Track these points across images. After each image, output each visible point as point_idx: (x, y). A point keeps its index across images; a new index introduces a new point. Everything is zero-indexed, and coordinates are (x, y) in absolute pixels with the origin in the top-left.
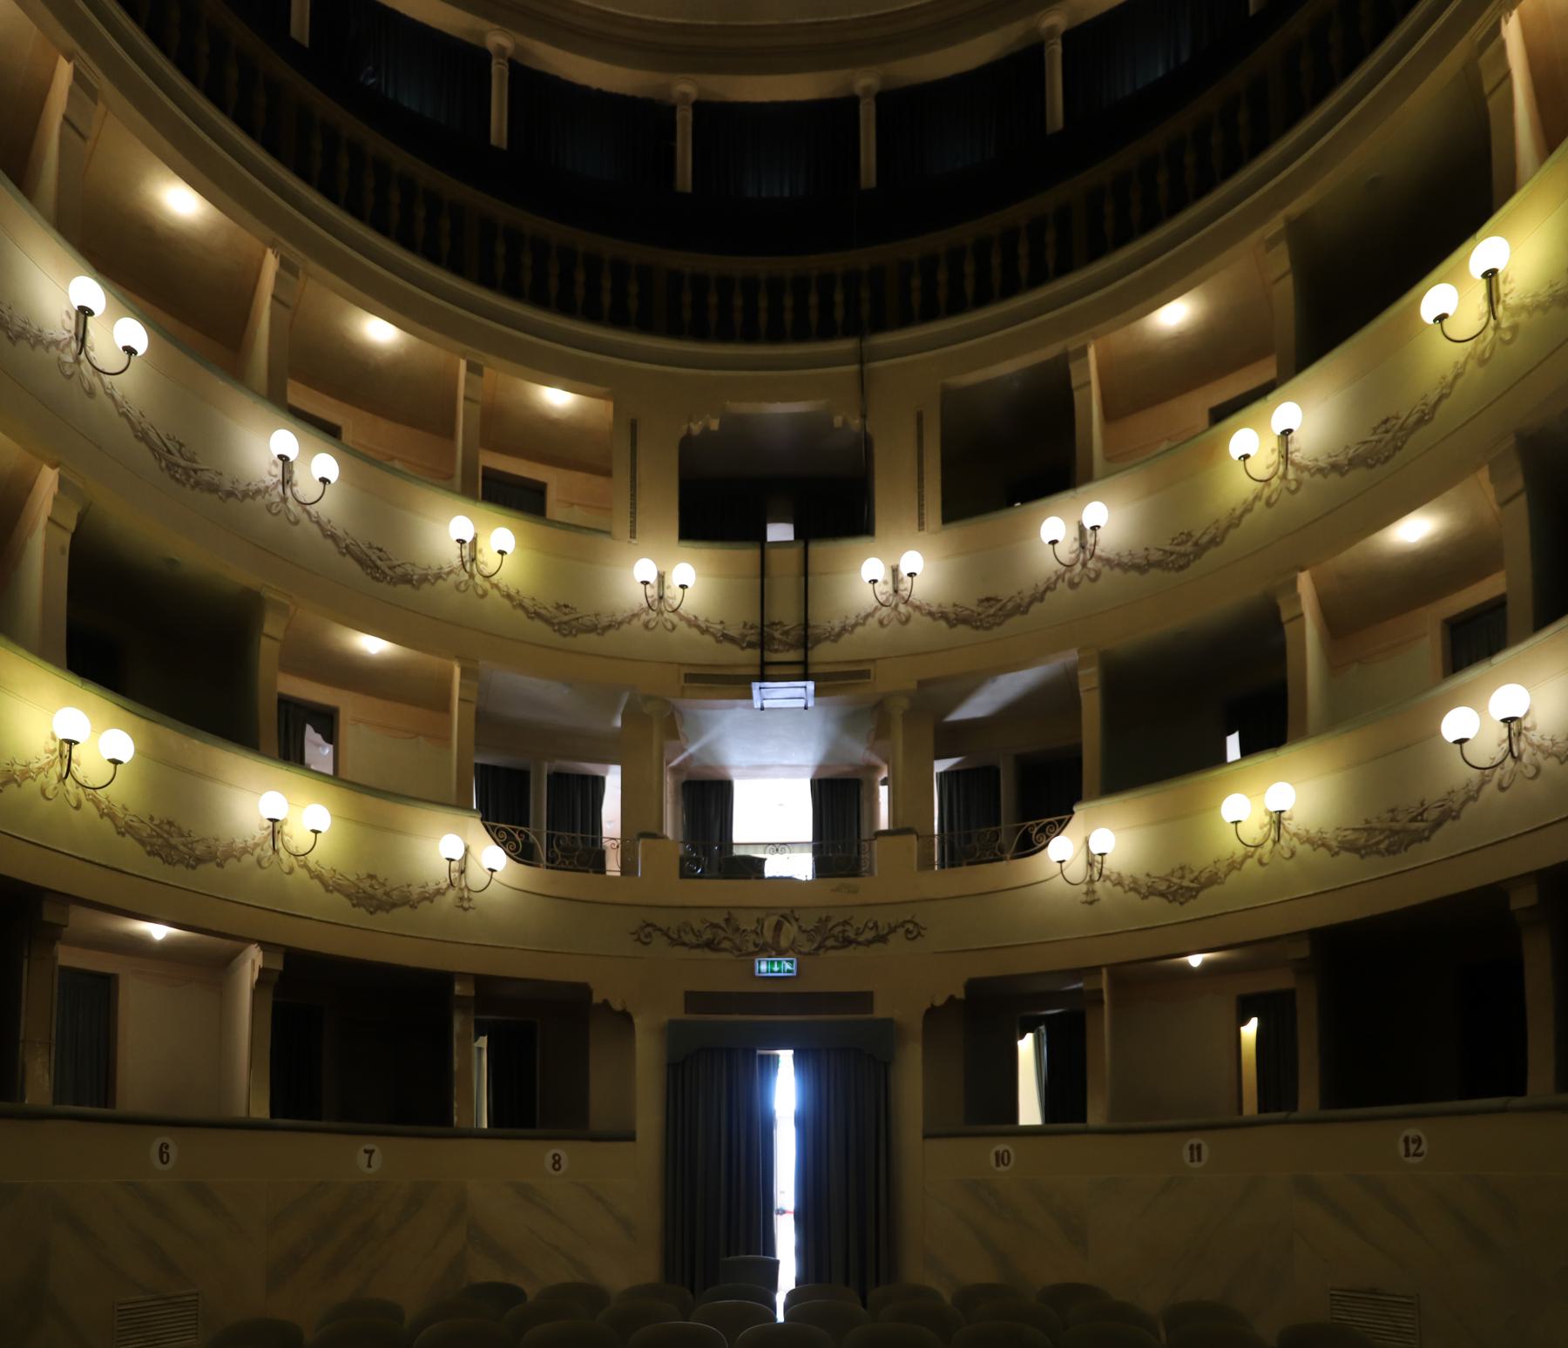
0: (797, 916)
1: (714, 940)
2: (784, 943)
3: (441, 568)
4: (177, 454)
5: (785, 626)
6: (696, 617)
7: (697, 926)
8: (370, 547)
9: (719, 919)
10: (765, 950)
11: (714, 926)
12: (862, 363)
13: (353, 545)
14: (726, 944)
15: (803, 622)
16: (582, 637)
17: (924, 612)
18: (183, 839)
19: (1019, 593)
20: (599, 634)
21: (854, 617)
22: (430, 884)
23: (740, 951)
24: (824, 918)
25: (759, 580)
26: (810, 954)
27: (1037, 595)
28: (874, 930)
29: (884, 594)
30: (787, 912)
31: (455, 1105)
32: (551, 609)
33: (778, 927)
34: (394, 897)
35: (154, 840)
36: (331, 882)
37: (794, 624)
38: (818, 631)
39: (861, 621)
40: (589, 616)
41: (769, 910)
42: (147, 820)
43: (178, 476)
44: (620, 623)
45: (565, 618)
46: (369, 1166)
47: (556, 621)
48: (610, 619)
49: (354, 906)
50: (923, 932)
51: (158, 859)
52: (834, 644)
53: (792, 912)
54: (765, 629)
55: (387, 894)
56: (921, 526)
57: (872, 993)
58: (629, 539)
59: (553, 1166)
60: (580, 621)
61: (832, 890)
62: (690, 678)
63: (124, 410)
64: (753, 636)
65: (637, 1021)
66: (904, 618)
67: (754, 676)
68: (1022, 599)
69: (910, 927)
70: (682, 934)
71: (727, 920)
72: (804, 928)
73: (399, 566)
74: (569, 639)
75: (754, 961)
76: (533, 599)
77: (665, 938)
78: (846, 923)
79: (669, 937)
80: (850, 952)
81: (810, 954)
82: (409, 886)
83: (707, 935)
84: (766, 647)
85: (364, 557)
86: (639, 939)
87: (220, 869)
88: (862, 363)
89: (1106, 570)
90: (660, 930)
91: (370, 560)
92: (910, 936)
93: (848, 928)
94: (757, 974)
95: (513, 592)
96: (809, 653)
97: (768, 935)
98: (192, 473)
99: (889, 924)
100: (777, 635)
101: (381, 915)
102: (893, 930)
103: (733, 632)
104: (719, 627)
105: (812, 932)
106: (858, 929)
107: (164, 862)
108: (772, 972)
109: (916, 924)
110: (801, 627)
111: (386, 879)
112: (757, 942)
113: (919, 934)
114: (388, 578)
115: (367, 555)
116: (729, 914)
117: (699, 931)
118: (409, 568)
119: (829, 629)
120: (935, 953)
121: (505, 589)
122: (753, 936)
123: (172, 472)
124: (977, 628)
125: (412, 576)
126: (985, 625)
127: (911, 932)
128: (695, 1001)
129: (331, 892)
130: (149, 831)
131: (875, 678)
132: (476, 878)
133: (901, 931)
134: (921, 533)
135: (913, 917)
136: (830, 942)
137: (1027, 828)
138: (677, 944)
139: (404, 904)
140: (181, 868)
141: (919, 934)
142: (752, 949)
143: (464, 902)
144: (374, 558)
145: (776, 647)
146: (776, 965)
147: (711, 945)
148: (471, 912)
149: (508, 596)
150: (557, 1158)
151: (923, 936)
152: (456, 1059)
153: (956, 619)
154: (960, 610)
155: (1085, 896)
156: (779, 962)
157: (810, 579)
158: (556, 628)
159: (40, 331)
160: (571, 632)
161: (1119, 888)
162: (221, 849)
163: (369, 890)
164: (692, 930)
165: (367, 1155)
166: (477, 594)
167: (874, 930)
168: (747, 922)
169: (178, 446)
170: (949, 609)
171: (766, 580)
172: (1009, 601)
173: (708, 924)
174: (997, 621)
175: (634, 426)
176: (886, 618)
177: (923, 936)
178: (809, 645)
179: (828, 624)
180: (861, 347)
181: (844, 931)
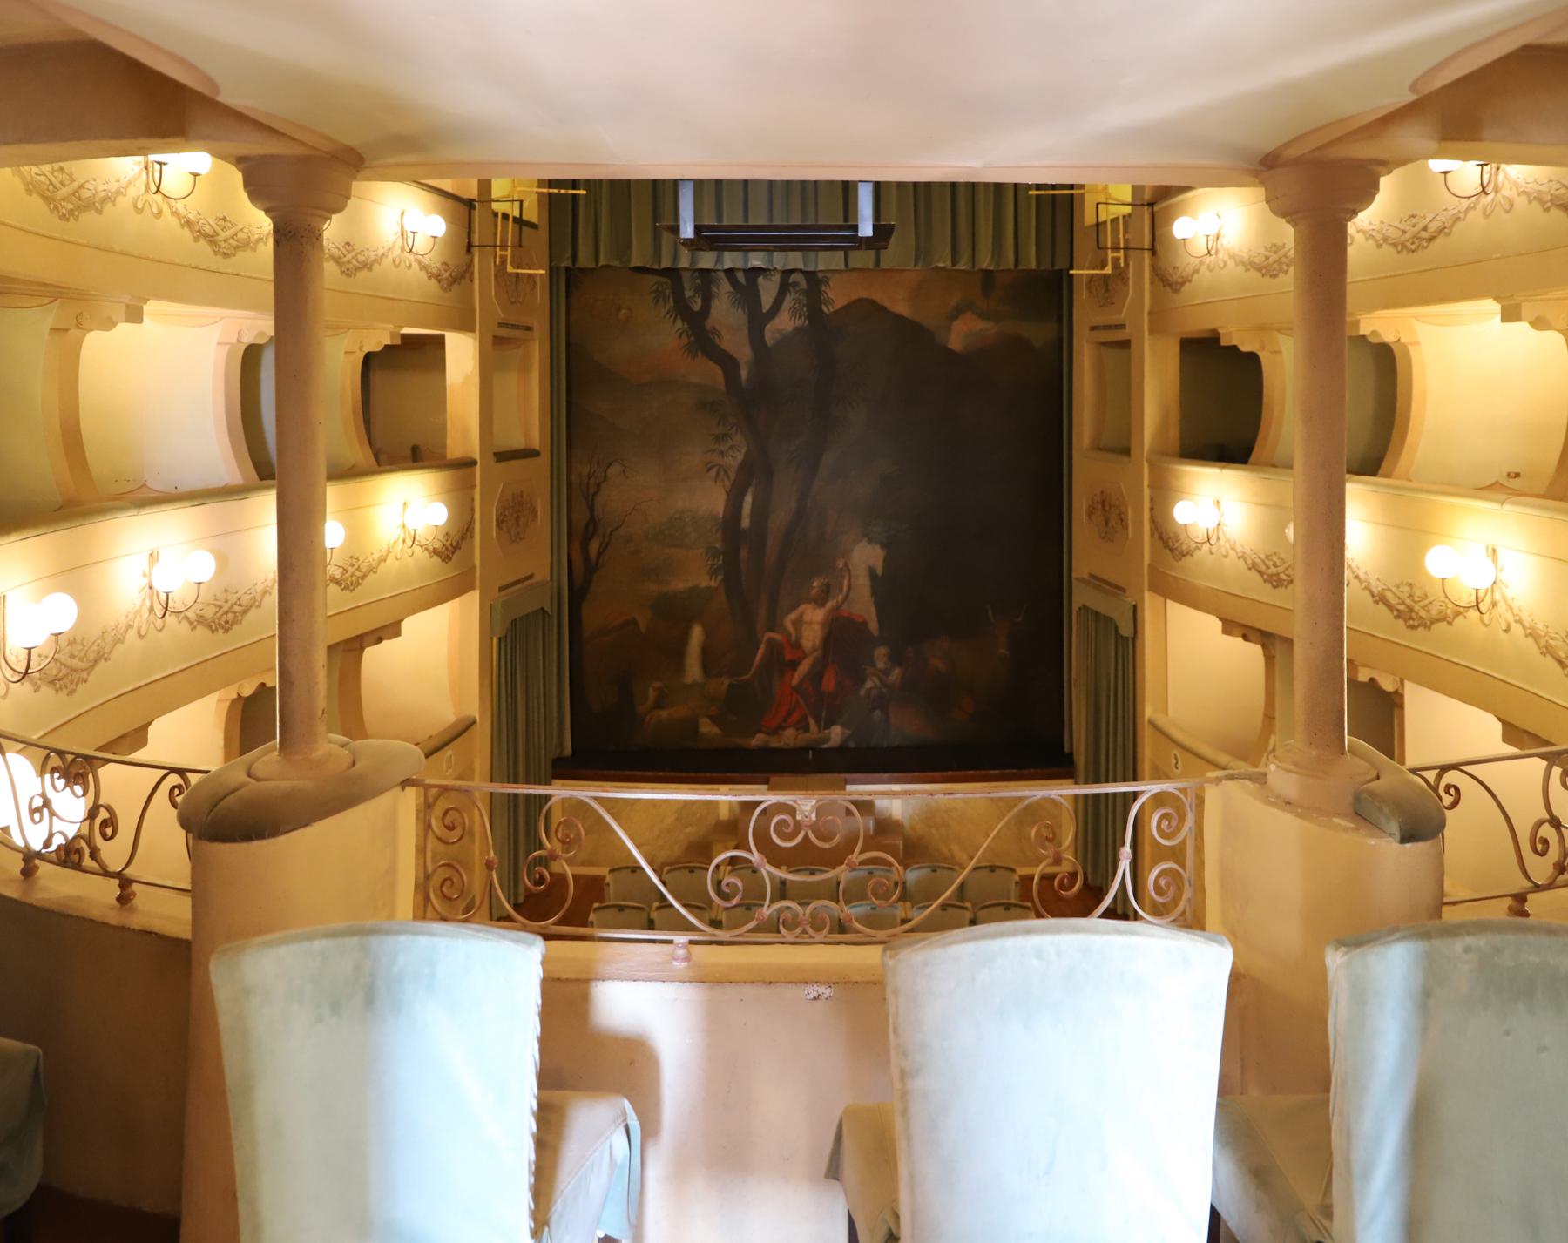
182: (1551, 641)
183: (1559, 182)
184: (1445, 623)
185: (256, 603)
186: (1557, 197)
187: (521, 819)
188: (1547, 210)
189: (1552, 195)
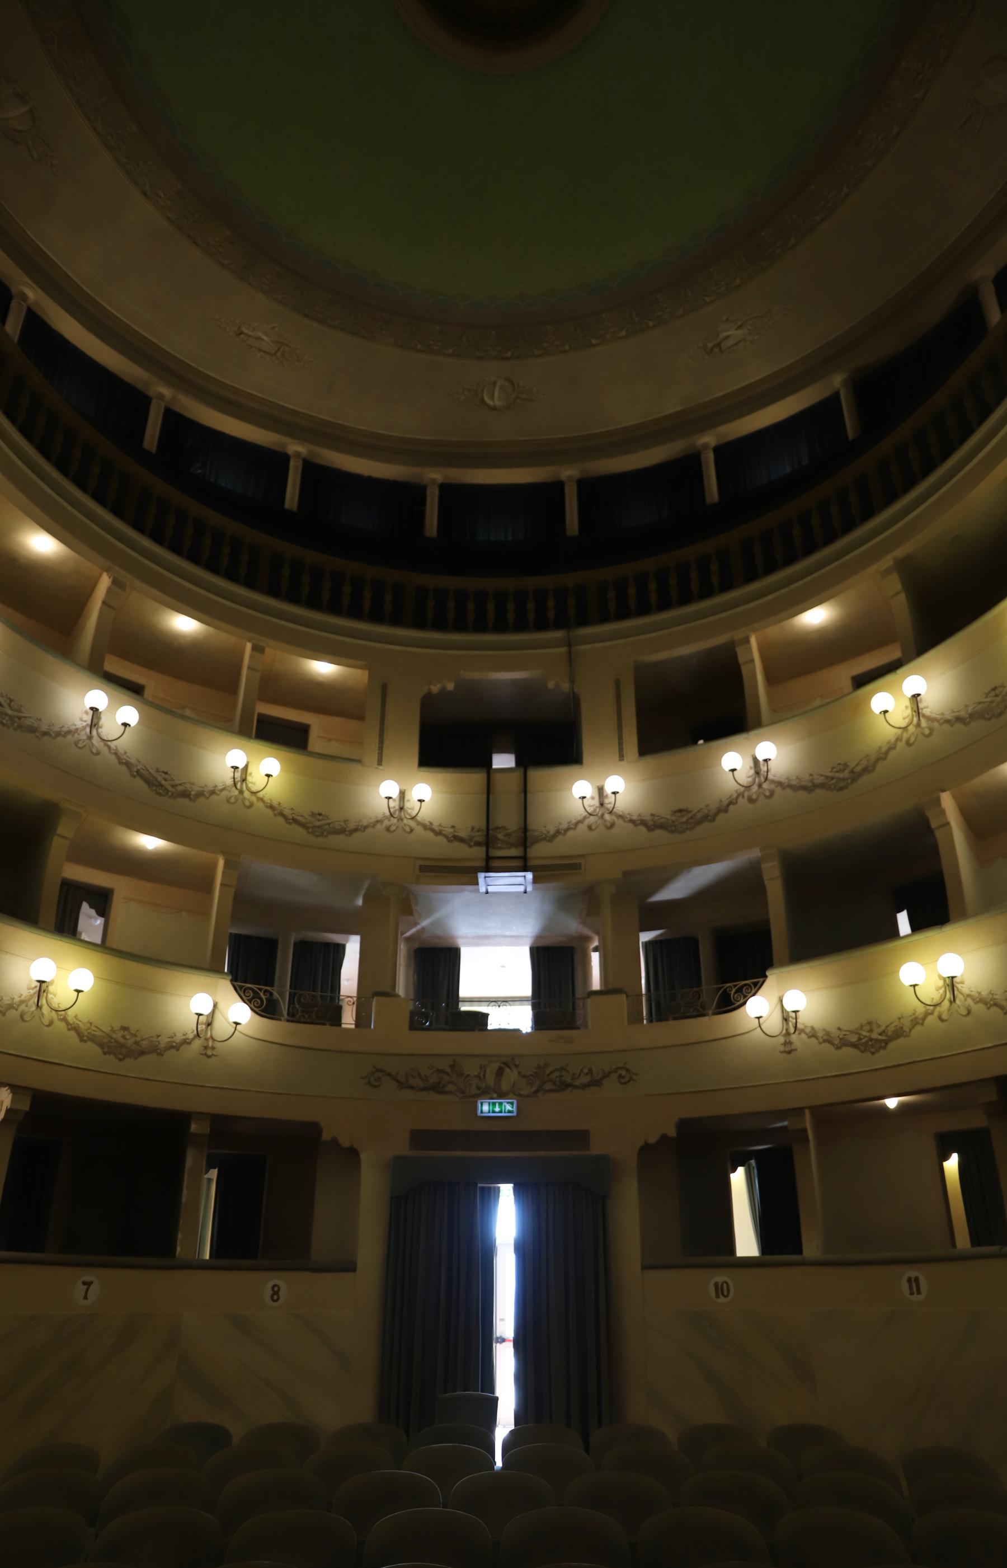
0: (517, 1063)
2: (505, 1086)
3: (216, 786)
8: (158, 771)
11: (440, 1071)
15: (522, 826)
17: (626, 820)
19: (707, 806)
20: (346, 835)
22: (177, 1035)
29: (591, 806)
31: (180, 1236)
32: (306, 816)
33: (500, 1073)
34: (143, 1046)
36: (86, 1034)
38: (536, 834)
39: (572, 826)
40: (339, 821)
43: (4, 721)
44: (365, 828)
45: (318, 823)
46: (86, 1298)
49: (105, 1053)
50: (634, 1077)
53: (513, 1059)
54: (490, 832)
55: (137, 1043)
56: (621, 757)
59: (272, 1297)
60: (331, 826)
62: (424, 869)
64: (480, 837)
65: (363, 1156)
66: (609, 825)
69: (623, 1073)
71: (452, 1067)
73: (180, 784)
74: (320, 839)
78: (562, 1069)
79: (398, 1081)
81: (528, 1096)
82: (158, 1036)
83: (433, 1079)
86: (369, 1083)
88: (570, 646)
90: (390, 1075)
91: (157, 780)
92: (623, 1081)
93: (564, 1073)
96: (528, 850)
97: (490, 1079)
98: (17, 719)
100: (500, 836)
101: (129, 1061)
102: (606, 1075)
103: (462, 834)
104: (451, 830)
105: (531, 1077)
108: (494, 1112)
109: (627, 1070)
113: (631, 1079)
114: (170, 794)
115: (154, 777)
118: (188, 786)
119: (546, 832)
121: (269, 801)
124: (672, 832)
125: (190, 792)
127: (624, 1077)
128: (420, 1138)
129: (85, 1041)
132: (222, 1028)
133: (614, 1076)
134: (621, 763)
135: (625, 1064)
139: (151, 1052)
141: (631, 1079)
144: (160, 779)
145: (500, 845)
146: (497, 1104)
150: (276, 1289)
151: (634, 1080)
155: (783, 1046)
156: (500, 1104)
157: (529, 795)
158: (310, 830)
161: (813, 1040)
163: (121, 1040)
165: (85, 1287)
169: (8, 701)
170: (648, 818)
171: (491, 796)
172: (699, 811)
173: (435, 1070)
178: (528, 844)
181: (561, 1076)
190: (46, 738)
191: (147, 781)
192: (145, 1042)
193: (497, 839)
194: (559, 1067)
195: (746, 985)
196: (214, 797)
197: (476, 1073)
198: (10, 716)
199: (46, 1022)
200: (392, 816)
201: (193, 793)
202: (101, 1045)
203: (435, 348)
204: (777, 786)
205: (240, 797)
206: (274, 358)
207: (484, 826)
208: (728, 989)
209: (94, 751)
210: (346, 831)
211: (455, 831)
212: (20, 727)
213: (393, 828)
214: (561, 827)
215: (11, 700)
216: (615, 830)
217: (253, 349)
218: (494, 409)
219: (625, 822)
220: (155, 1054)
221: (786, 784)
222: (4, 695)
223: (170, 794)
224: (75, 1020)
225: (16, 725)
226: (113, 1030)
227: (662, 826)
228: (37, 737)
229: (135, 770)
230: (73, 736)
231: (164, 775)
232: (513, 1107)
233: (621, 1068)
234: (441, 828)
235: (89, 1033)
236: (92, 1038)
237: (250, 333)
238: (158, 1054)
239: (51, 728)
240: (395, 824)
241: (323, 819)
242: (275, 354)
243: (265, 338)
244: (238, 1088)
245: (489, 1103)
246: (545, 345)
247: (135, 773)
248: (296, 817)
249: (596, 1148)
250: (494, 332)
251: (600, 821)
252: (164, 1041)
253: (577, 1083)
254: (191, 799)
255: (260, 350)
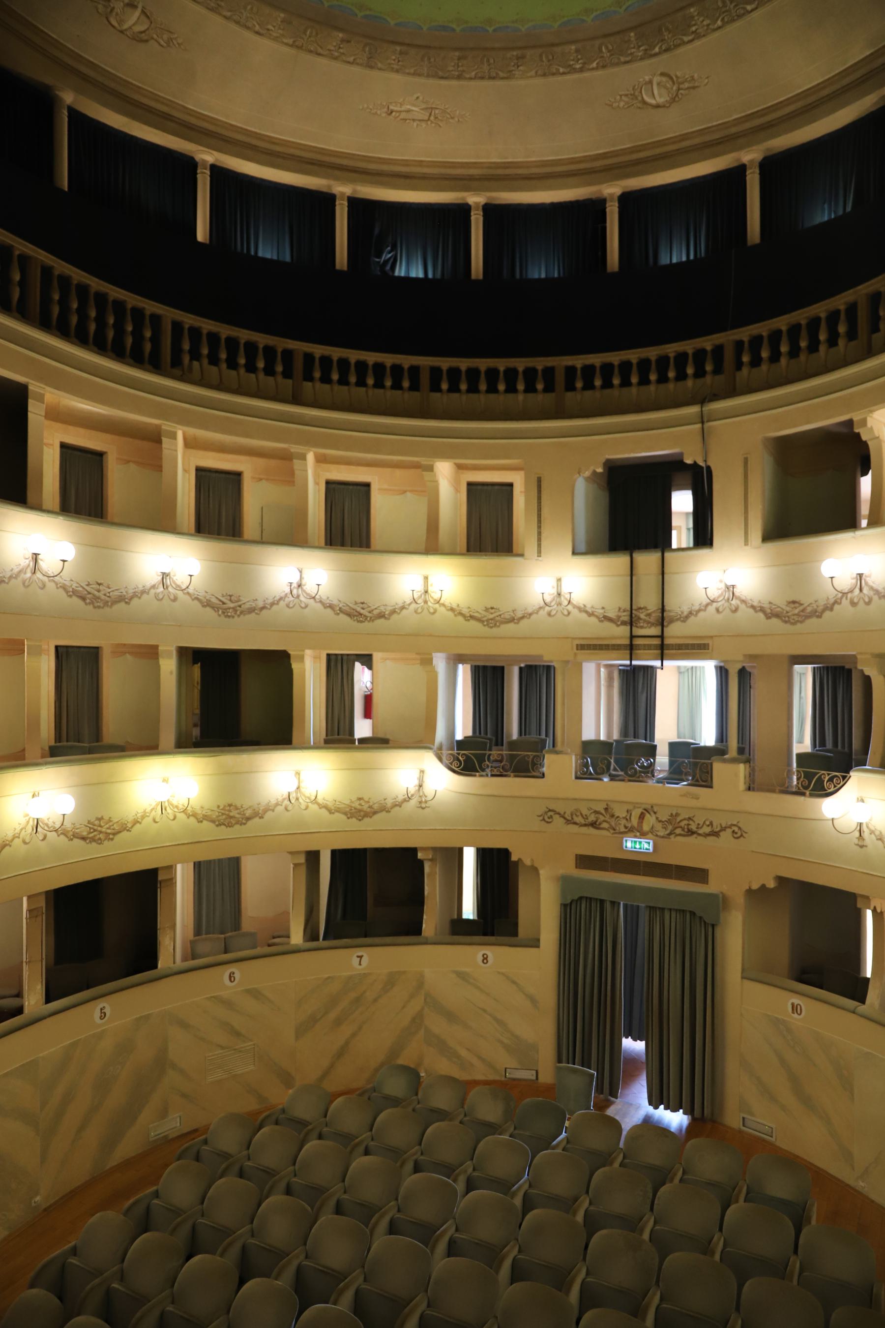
0: (655, 810)
1: (596, 821)
2: (646, 828)
3: (405, 602)
4: (228, 602)
5: (647, 610)
6: (585, 606)
7: (585, 812)
8: (356, 603)
9: (600, 808)
10: (630, 831)
11: (596, 812)
12: (703, 423)
13: (344, 606)
14: (605, 825)
15: (661, 607)
16: (503, 626)
17: (748, 605)
18: (238, 811)
19: (816, 602)
20: (515, 623)
21: (698, 604)
22: (399, 796)
23: (614, 830)
24: (674, 814)
25: (629, 578)
26: (663, 837)
27: (828, 605)
28: (710, 826)
29: (719, 589)
30: (649, 807)
31: (425, 917)
32: (481, 612)
33: (642, 817)
34: (375, 808)
35: (220, 818)
36: (333, 808)
37: (655, 609)
38: (672, 614)
39: (703, 608)
40: (508, 612)
41: (635, 805)
42: (216, 809)
43: (229, 614)
44: (530, 615)
45: (491, 616)
46: (360, 964)
47: (485, 619)
48: (523, 612)
49: (348, 818)
50: (744, 834)
51: (223, 827)
52: (683, 624)
53: (652, 807)
54: (634, 612)
55: (370, 807)
56: (746, 543)
57: (708, 870)
58: (537, 558)
59: (487, 957)
60: (502, 616)
61: (681, 796)
62: (581, 647)
63: (196, 596)
64: (627, 619)
65: (541, 872)
66: (734, 609)
67: (624, 645)
68: (817, 606)
69: (736, 829)
70: (574, 817)
71: (606, 809)
72: (660, 819)
73: (376, 609)
74: (494, 629)
75: (623, 838)
76: (469, 608)
77: (562, 819)
78: (690, 819)
79: (565, 818)
80: (692, 839)
81: (663, 837)
82: (385, 799)
83: (592, 818)
84: (634, 624)
85: (352, 611)
86: (544, 820)
87: (261, 820)
88: (703, 423)
89: (876, 598)
90: (559, 814)
91: (356, 611)
92: (735, 836)
93: (691, 822)
94: (624, 848)
95: (454, 606)
96: (665, 629)
97: (635, 821)
98: (238, 608)
99: (721, 825)
100: (642, 616)
101: (366, 820)
102: (723, 829)
103: (612, 615)
104: (602, 611)
105: (666, 823)
106: (698, 824)
107: (227, 827)
108: (635, 848)
109: (740, 828)
110: (660, 611)
111: (369, 798)
112: (627, 825)
113: (742, 835)
114: (368, 619)
115: (354, 610)
116: (607, 805)
117: (586, 815)
118: (382, 608)
119: (680, 613)
120: (753, 851)
121: (449, 605)
122: (623, 822)
123: (226, 614)
124: (786, 622)
125: (385, 612)
126: (792, 621)
127: (736, 833)
128: (585, 861)
129: (333, 813)
130: (217, 814)
131: (712, 651)
132: (429, 788)
133: (729, 831)
134: (747, 548)
135: (738, 822)
136: (678, 831)
137: (821, 776)
138: (571, 823)
139: (382, 811)
140: (237, 827)
141: (742, 835)
142: (623, 829)
143: (423, 804)
144: (359, 609)
145: (642, 624)
146: (638, 843)
147: (594, 825)
148: (427, 810)
149: (452, 609)
150: (485, 956)
151: (744, 837)
152: (426, 888)
153: (771, 613)
154: (774, 607)
155: (857, 840)
156: (640, 842)
157: (666, 576)
158: (485, 623)
159: (144, 587)
160: (496, 624)
161: (880, 842)
162: (261, 808)
163: (359, 807)
164: (581, 814)
165: (359, 959)
166: (430, 613)
167: (710, 826)
168: (621, 812)
169: (229, 598)
170: (766, 606)
171: (634, 578)
172: (808, 605)
173: (592, 811)
174: (800, 619)
175: (539, 480)
176: (721, 607)
177: (744, 837)
178: (665, 624)
179: (679, 609)
180: (702, 411)
181: (688, 825)
182: (76, 831)
183: (78, 583)
184: (126, 831)
185: (455, 464)
186: (76, 590)
187: (650, 1008)
188: (57, 588)
189: (73, 589)
190: (264, 611)
191: (349, 615)
192: (376, 805)
193: (639, 618)
194: (687, 817)
195: (836, 776)
196: (404, 611)
197: (624, 816)
198: (233, 608)
199: (303, 807)
200: (547, 605)
201: (387, 613)
202: (345, 814)
203: (578, 66)
204: (875, 594)
205: (426, 606)
206: (429, 123)
207: (628, 607)
208: (823, 777)
209: (303, 605)
210: (514, 619)
211: (605, 612)
212: (241, 613)
213: (553, 613)
214: (693, 608)
215: (231, 596)
216: (739, 614)
217: (408, 121)
218: (658, 106)
219: (747, 607)
220: (384, 813)
221: (882, 594)
222: (225, 594)
223: (368, 619)
224: (323, 801)
225: (238, 613)
226: (352, 802)
227: (777, 615)
228: (257, 614)
229: (338, 608)
230: (284, 601)
231: (362, 605)
232: (649, 846)
233: (734, 825)
234: (593, 609)
235: (335, 807)
236: (338, 810)
237: (399, 109)
238: (387, 812)
239: (266, 602)
240: (555, 609)
241: (495, 612)
242: (429, 119)
243: (414, 108)
244: (447, 828)
245: (632, 841)
246: (694, 29)
247: (338, 612)
248: (472, 614)
249: (712, 887)
250: (632, 34)
251: (726, 604)
252: (389, 802)
253: (701, 831)
254: (386, 618)
255: (414, 120)
